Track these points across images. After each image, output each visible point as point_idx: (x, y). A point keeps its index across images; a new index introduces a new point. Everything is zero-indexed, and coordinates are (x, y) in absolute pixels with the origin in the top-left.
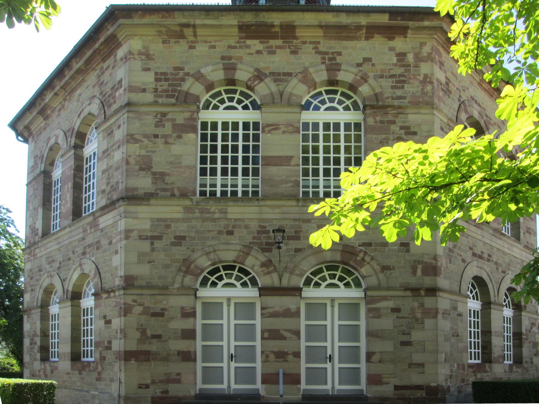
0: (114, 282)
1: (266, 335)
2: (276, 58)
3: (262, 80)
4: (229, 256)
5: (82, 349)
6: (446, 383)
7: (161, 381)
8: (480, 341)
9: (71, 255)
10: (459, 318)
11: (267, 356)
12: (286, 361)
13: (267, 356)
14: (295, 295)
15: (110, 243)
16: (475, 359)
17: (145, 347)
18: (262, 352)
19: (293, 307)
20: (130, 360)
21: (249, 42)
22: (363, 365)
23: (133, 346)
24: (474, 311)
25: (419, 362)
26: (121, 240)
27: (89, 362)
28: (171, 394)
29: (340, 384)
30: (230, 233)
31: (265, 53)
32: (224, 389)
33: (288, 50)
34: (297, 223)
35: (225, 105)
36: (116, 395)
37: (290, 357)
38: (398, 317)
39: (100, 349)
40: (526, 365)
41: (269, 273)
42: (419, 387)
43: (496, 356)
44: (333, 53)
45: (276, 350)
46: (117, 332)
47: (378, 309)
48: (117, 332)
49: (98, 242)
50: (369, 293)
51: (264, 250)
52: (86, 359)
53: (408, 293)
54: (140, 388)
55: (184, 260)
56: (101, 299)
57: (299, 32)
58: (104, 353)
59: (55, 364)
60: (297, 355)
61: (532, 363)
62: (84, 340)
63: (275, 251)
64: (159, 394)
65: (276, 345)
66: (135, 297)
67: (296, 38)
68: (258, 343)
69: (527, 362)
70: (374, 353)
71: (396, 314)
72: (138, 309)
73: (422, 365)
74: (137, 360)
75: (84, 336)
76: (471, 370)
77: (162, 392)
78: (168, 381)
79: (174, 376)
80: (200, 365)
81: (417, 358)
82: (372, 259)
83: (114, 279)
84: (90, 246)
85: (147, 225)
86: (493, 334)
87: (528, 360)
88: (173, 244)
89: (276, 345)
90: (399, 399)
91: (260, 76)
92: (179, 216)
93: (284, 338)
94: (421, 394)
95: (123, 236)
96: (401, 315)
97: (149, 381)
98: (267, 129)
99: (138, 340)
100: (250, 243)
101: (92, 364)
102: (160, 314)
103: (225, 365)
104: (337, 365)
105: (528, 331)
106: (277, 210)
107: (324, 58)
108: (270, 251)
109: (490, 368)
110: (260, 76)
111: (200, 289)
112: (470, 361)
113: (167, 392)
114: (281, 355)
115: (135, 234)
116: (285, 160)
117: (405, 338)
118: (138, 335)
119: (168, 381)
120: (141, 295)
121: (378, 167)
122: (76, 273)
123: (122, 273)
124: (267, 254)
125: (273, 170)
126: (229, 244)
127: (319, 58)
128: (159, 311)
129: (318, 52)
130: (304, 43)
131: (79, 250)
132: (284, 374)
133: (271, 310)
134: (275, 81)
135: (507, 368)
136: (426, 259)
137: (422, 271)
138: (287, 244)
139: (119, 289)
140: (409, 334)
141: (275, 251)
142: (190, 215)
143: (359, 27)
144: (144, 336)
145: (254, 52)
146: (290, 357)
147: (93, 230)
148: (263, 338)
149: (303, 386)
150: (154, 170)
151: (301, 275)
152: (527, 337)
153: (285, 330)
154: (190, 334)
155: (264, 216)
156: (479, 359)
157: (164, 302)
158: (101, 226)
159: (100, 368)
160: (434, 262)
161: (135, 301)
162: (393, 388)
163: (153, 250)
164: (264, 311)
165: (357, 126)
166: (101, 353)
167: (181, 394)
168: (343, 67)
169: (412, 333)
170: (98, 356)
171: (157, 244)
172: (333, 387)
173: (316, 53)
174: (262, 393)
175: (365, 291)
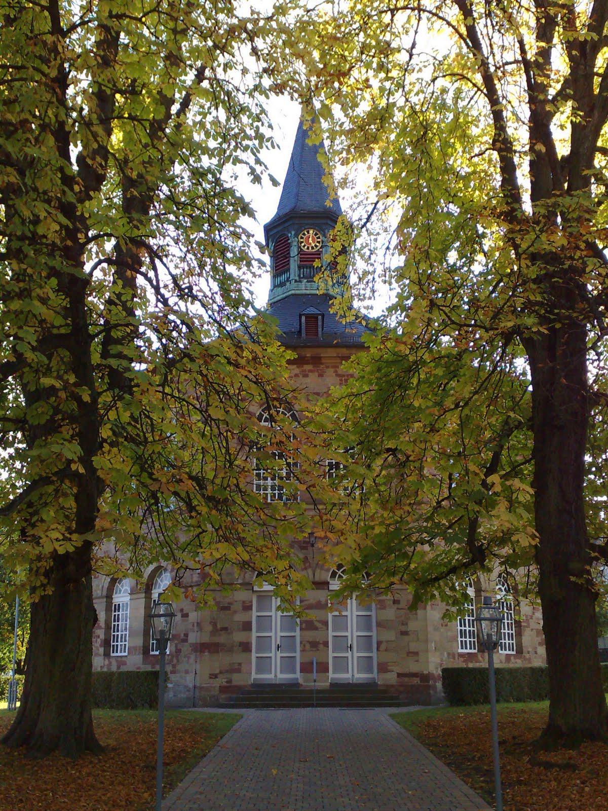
0: (192, 578)
1: (304, 626)
2: (308, 380)
6: (437, 672)
7: (227, 671)
13: (304, 646)
14: (324, 589)
17: (216, 639)
18: (301, 643)
19: (323, 600)
20: (204, 652)
23: (206, 639)
25: (415, 651)
28: (234, 683)
30: (422, 799)
31: (301, 376)
32: (272, 679)
33: (317, 374)
36: (191, 685)
37: (321, 646)
38: (398, 609)
40: (527, 656)
41: (306, 569)
42: (415, 675)
45: (311, 640)
46: (193, 625)
47: (383, 601)
48: (193, 625)
54: (210, 678)
57: (323, 361)
58: (179, 647)
59: (124, 659)
60: (326, 644)
61: (536, 653)
63: (310, 548)
64: (225, 684)
67: (322, 364)
69: (528, 652)
71: (396, 606)
73: (416, 654)
74: (209, 652)
76: (462, 659)
77: (227, 682)
79: (236, 666)
80: (254, 655)
81: (413, 647)
87: (530, 650)
93: (316, 629)
94: (416, 681)
96: (400, 606)
97: (217, 671)
99: (211, 632)
102: (226, 608)
104: (356, 655)
105: (529, 617)
107: (341, 380)
108: (305, 548)
112: (460, 651)
113: (230, 681)
114: (314, 645)
117: (403, 628)
118: (210, 628)
121: (476, 89)
129: (338, 375)
130: (328, 367)
133: (306, 603)
135: (503, 658)
141: (310, 548)
144: (215, 631)
146: (321, 646)
149: (331, 675)
151: (328, 570)
152: (529, 624)
154: (247, 626)
156: (475, 649)
159: (175, 660)
162: (396, 675)
166: (176, 646)
167: (241, 683)
174: (301, 681)
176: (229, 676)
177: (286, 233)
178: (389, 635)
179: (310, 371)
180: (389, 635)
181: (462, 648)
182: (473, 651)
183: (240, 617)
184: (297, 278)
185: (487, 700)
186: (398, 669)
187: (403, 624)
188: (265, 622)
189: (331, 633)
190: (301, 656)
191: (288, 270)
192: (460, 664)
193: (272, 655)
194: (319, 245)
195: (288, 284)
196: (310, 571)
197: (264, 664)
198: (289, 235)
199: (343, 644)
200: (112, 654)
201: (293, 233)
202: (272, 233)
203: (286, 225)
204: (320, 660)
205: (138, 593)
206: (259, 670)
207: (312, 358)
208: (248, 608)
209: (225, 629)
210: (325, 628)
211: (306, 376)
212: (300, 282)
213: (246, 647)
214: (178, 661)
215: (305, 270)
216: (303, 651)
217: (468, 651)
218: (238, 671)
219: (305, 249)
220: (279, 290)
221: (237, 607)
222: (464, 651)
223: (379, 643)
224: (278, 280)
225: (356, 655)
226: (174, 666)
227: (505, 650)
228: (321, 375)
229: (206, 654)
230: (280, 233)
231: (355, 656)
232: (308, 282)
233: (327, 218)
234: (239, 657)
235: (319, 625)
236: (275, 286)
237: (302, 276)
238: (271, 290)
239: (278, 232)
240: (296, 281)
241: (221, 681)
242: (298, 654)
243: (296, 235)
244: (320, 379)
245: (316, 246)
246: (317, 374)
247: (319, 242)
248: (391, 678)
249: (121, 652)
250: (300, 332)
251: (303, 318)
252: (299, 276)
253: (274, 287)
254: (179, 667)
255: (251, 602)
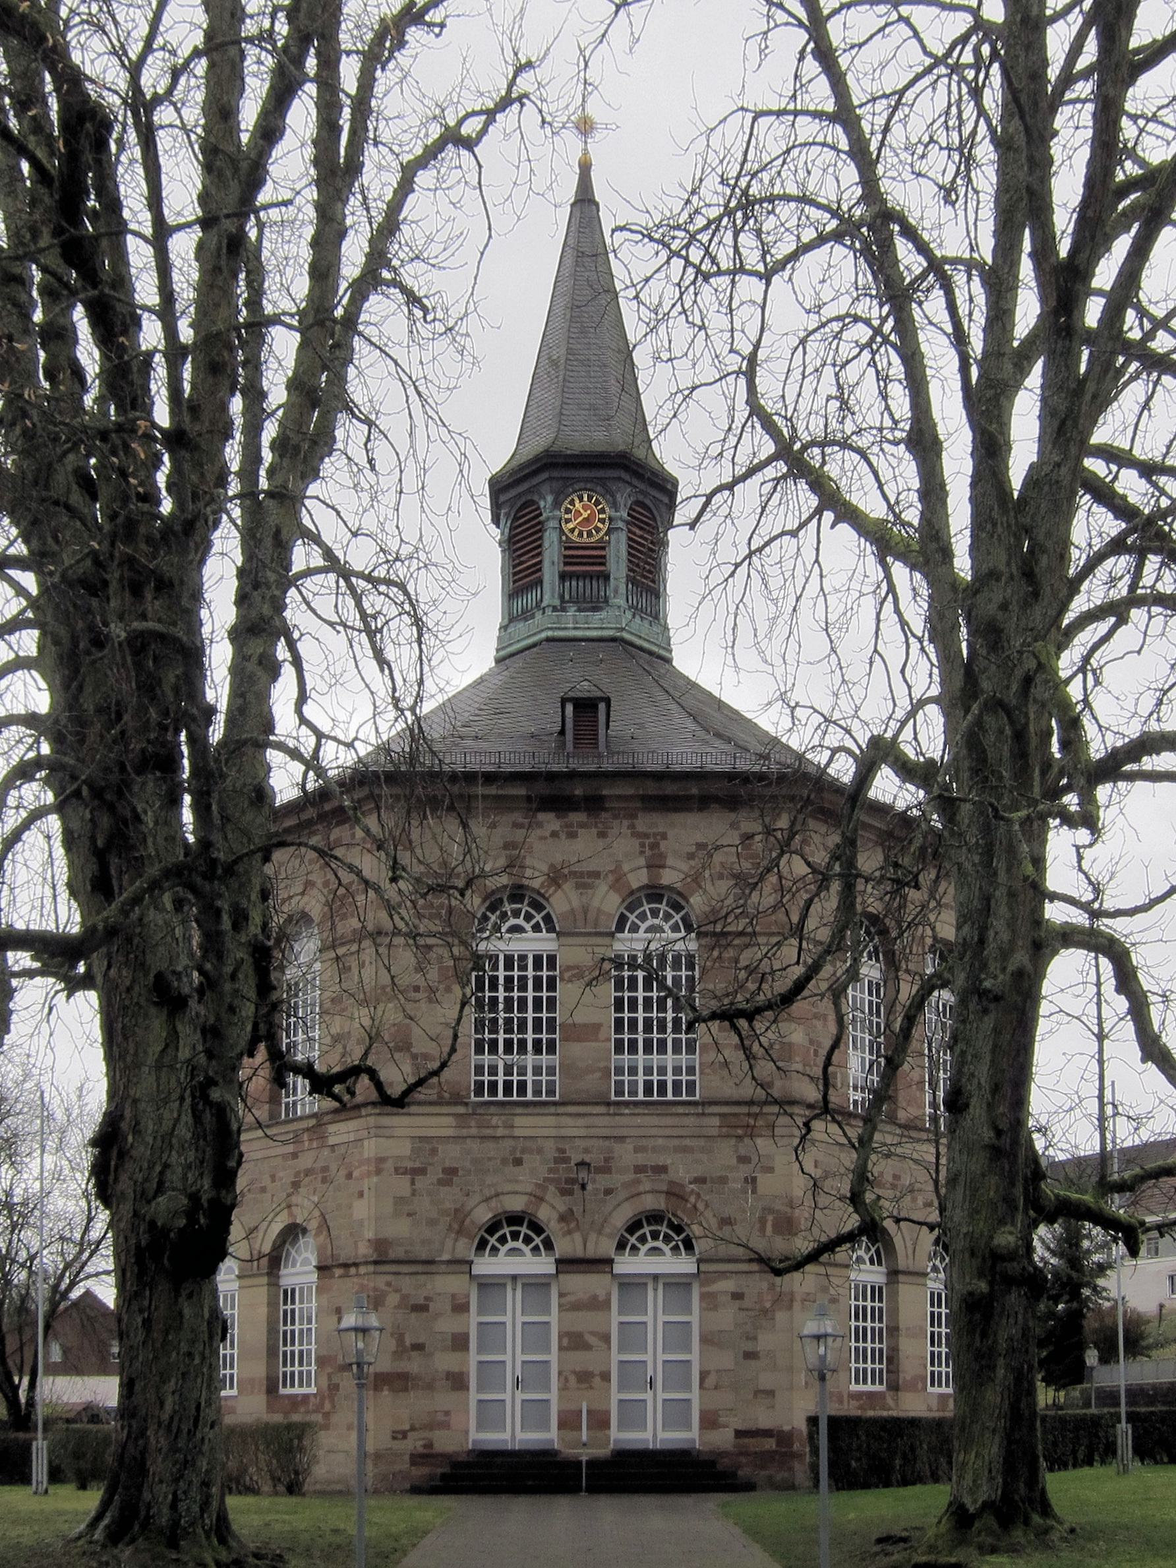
0: (356, 1247)
1: (565, 1342)
3: (559, 886)
4: (516, 1204)
5: (282, 1369)
8: (884, 1346)
9: (266, 1181)
10: (833, 1306)
11: (566, 1380)
12: (591, 1388)
13: (566, 1380)
15: (349, 1176)
16: (873, 1382)
18: (560, 1373)
21: (541, 816)
22: (695, 1395)
24: (873, 1288)
25: (768, 1388)
26: (369, 1174)
27: (306, 1397)
29: (665, 1427)
32: (506, 1441)
34: (607, 1143)
35: (508, 924)
39: (329, 1370)
41: (569, 1232)
42: (767, 1433)
43: (908, 1378)
44: (655, 835)
49: (325, 1169)
50: (703, 1267)
51: (564, 1192)
52: (289, 1391)
53: (755, 1267)
54: (394, 1438)
55: (456, 1210)
56: (332, 1277)
60: (606, 1377)
62: (285, 1353)
64: (421, 1450)
65: (580, 1360)
66: (389, 1278)
68: (553, 1357)
70: (708, 1372)
72: (393, 1299)
73: (771, 1393)
74: (392, 1390)
75: (285, 1345)
77: (425, 1446)
78: (431, 1426)
79: (440, 1417)
80: (474, 1396)
81: (766, 1380)
82: (707, 1206)
83: (356, 1243)
84: (308, 1172)
85: (403, 1149)
86: (903, 1332)
88: (441, 1182)
89: (580, 1360)
90: (741, 1454)
91: (556, 877)
92: (450, 1132)
93: (587, 1347)
94: (770, 1444)
95: (372, 1168)
97: (407, 1427)
98: (567, 975)
99: (395, 1353)
100: (545, 1179)
101: (312, 1399)
103: (507, 1396)
104: (661, 1396)
106: (581, 1122)
107: (642, 845)
108: (570, 1193)
109: (896, 1401)
110: (556, 877)
111: (476, 1260)
112: (854, 1387)
113: (429, 1445)
114: (584, 1377)
115: (389, 1165)
116: (590, 1031)
117: (749, 1346)
119: (431, 1426)
120: (398, 1273)
122: (278, 1219)
123: (369, 1234)
124: (567, 1198)
125: (577, 1050)
126: (517, 1181)
127: (636, 842)
128: (422, 1302)
131: (286, 1176)
132: (588, 1412)
134: (578, 886)
136: (779, 1206)
137: (774, 1225)
138: (594, 1181)
139: (366, 1263)
140: (755, 1338)
142: (464, 1132)
143: (689, 798)
144: (402, 1350)
145: (547, 834)
147: (315, 1145)
148: (561, 1348)
150: (414, 1050)
153: (592, 1333)
154: (460, 1343)
155: (564, 1132)
157: (429, 1286)
158: (332, 1141)
159: (327, 1406)
160: (788, 1210)
161: (389, 1284)
163: (414, 1193)
164: (563, 1300)
165: (690, 958)
166: (329, 1376)
168: (670, 861)
169: (760, 1337)
170: (324, 1383)
171: (422, 1182)
172: (655, 1435)
173: (633, 834)
175: (699, 1261)
176: (426, 1434)
177: (536, 498)
178: (725, 1360)
179: (582, 825)
180: (725, 1360)
181: (857, 1382)
182: (877, 1388)
183: (448, 1325)
184: (557, 602)
185: (834, 1422)
186: (737, 1422)
187: (748, 1338)
188: (633, 1336)
189: (615, 1357)
190: (560, 1398)
191: (540, 582)
192: (851, 1409)
193: (507, 1396)
194: (604, 528)
195: (539, 615)
196: (577, 1237)
197: (490, 1413)
198: (542, 504)
199: (633, 1375)
200: (282, 1391)
201: (550, 498)
202: (502, 498)
203: (535, 481)
204: (596, 1406)
205: (253, 1276)
206: (481, 1427)
207: (586, 799)
208: (461, 1308)
209: (418, 1347)
210: (605, 1346)
211: (572, 835)
212: (563, 609)
213: (458, 1382)
214: (334, 1407)
215: (574, 583)
216: (563, 1388)
217: (869, 1387)
218: (445, 1425)
219: (574, 537)
220: (520, 627)
221: (441, 1305)
222: (861, 1388)
223: (703, 1375)
224: (519, 604)
225: (661, 1396)
226: (327, 1415)
227: (940, 1385)
228: (602, 835)
229: (386, 1393)
230: (523, 500)
231: (654, 1401)
232: (579, 610)
233: (626, 468)
234: (444, 1400)
235: (592, 1340)
236: (511, 618)
237: (567, 597)
238: (503, 628)
239: (520, 495)
240: (555, 609)
241: (414, 1443)
242: (553, 1396)
243: (557, 504)
244: (601, 843)
245: (598, 530)
246: (594, 831)
247: (602, 521)
248: (723, 1439)
249: (301, 1385)
250: (562, 732)
251: (569, 708)
252: (562, 597)
253: (511, 621)
254: (335, 1419)
255: (468, 1296)
